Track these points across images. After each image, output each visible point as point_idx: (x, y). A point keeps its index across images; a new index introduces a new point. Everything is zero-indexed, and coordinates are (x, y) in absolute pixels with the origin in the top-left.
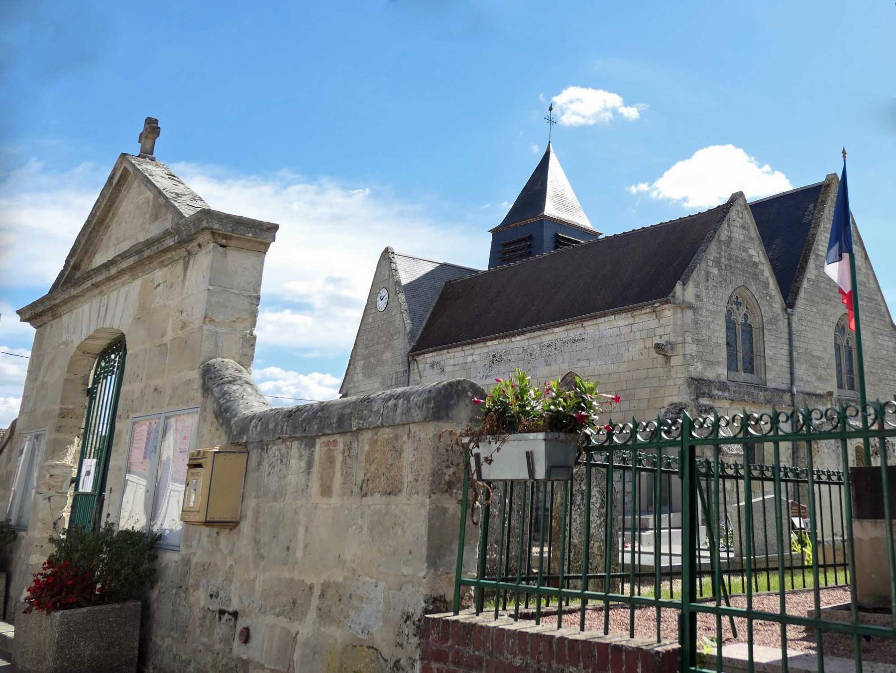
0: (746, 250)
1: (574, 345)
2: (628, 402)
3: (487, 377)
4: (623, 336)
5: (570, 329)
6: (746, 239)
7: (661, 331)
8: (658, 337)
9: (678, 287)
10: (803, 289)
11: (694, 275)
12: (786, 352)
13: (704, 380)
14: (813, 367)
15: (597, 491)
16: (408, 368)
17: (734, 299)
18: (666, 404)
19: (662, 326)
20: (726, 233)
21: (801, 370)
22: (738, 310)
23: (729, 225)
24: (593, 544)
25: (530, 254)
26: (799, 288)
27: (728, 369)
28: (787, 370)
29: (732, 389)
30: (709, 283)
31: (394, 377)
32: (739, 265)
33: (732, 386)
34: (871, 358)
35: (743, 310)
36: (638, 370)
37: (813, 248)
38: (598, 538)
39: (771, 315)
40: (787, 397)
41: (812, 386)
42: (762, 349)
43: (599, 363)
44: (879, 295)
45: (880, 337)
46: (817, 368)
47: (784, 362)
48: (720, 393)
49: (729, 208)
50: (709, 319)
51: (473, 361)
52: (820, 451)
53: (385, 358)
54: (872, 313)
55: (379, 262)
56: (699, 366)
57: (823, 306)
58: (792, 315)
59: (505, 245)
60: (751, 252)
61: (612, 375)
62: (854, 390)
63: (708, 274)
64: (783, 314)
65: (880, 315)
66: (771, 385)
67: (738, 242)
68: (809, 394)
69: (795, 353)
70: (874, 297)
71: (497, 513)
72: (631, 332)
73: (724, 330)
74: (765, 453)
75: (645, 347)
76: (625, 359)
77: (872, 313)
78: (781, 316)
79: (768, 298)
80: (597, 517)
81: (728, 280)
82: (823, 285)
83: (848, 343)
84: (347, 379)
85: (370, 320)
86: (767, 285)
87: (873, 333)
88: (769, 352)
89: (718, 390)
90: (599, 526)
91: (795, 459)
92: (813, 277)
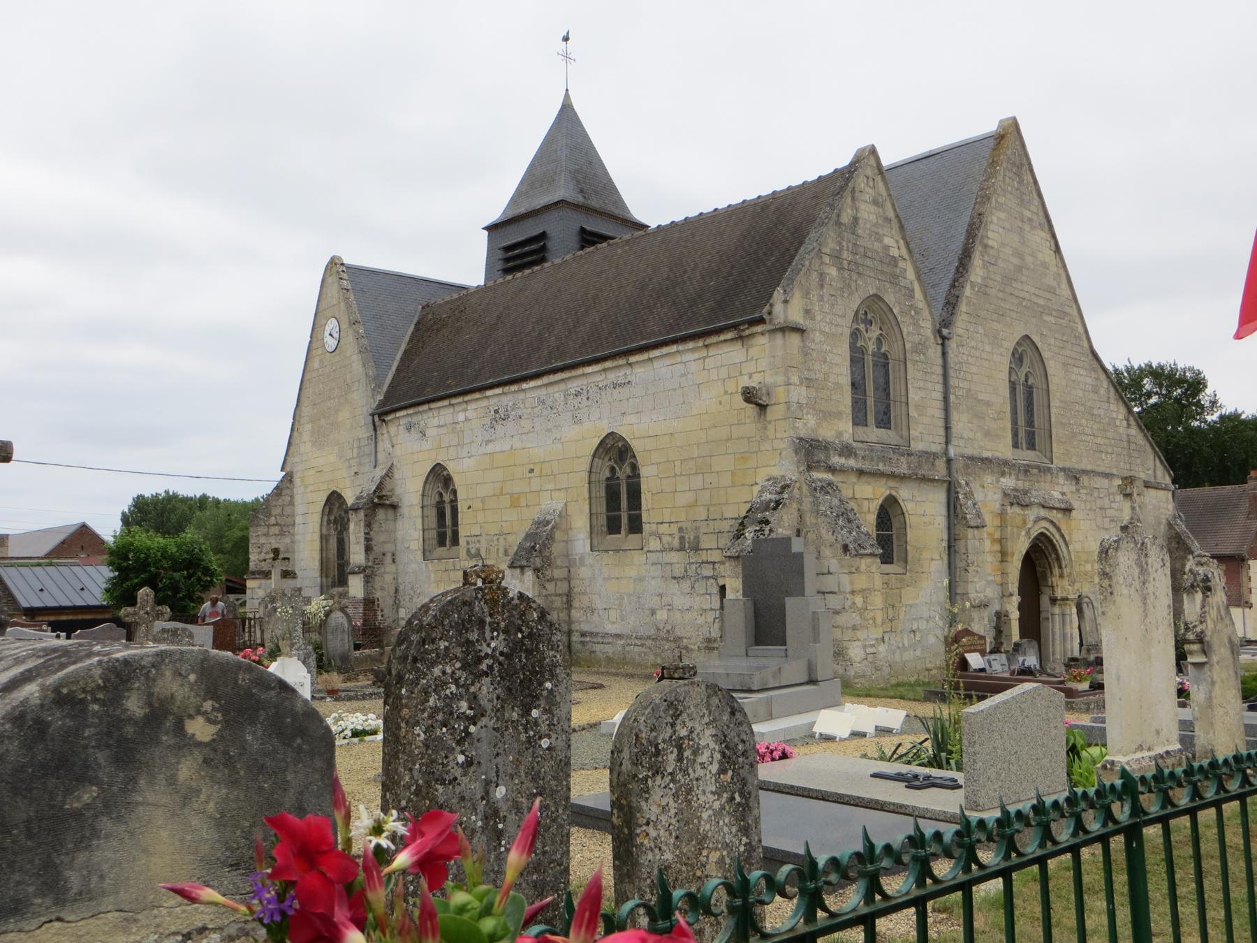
0: (879, 238)
1: (616, 392)
3: (488, 442)
4: (690, 376)
6: (880, 222)
7: (749, 367)
8: (746, 377)
9: (778, 294)
10: (964, 298)
11: (801, 277)
12: (939, 396)
13: (818, 441)
15: (713, 736)
16: (373, 433)
17: (861, 315)
19: (752, 359)
20: (849, 211)
21: (960, 422)
22: (867, 331)
23: (853, 198)
24: (707, 857)
25: (543, 260)
26: (958, 297)
27: (855, 424)
28: (941, 423)
29: (860, 453)
33: (860, 449)
34: (1061, 401)
35: (874, 332)
37: (980, 234)
38: (718, 842)
39: (916, 339)
40: (941, 464)
42: (903, 393)
43: (654, 417)
45: (1075, 369)
47: (936, 410)
48: (842, 461)
50: (824, 347)
51: (467, 420)
52: (1115, 593)
53: (340, 419)
57: (995, 324)
59: (508, 249)
61: (676, 436)
62: (1035, 449)
63: (822, 276)
64: (935, 337)
65: (1075, 337)
66: (917, 446)
67: (868, 226)
68: (972, 458)
69: (952, 397)
70: (1067, 309)
71: (479, 824)
73: (848, 363)
75: (726, 393)
76: (695, 411)
79: (913, 313)
80: (713, 793)
81: (853, 284)
82: (993, 292)
83: (1026, 380)
85: (317, 365)
87: (1065, 365)
88: (914, 396)
89: (840, 455)
90: (719, 813)
92: (979, 281)
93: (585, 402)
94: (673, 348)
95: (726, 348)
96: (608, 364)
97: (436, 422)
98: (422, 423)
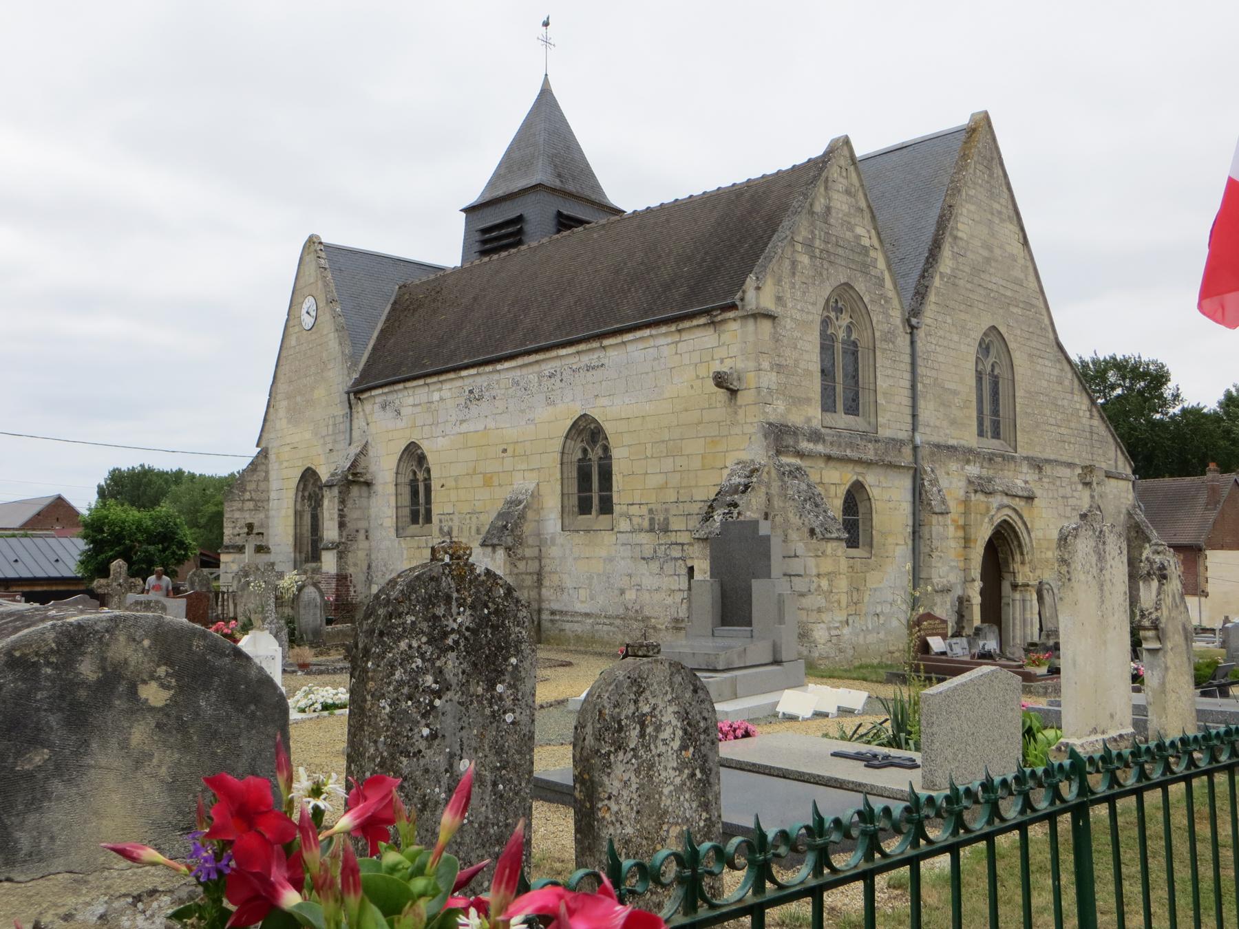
0: (851, 229)
1: (589, 374)
2: (672, 459)
3: (462, 422)
4: (663, 360)
5: (684, 329)
6: (852, 211)
7: (722, 352)
8: (718, 362)
11: (773, 265)
12: (907, 384)
13: (787, 426)
14: (944, 405)
15: (675, 713)
16: (348, 410)
17: (832, 303)
18: (730, 462)
19: (724, 344)
20: (822, 200)
21: (927, 411)
22: (837, 319)
23: (826, 188)
24: (668, 831)
28: (908, 411)
30: (797, 278)
31: (331, 423)
32: (840, 251)
36: (686, 410)
38: (678, 816)
39: (886, 327)
40: (907, 451)
41: (941, 434)
42: (872, 380)
43: (627, 400)
44: (1041, 299)
45: (1040, 360)
46: (950, 407)
47: (904, 398)
48: (811, 446)
49: (827, 162)
51: (442, 399)
54: (1030, 326)
55: (301, 259)
56: (780, 406)
57: (963, 314)
58: (917, 328)
59: (485, 231)
60: (859, 231)
63: (794, 264)
65: (1041, 329)
66: (885, 433)
67: (840, 216)
68: (938, 446)
69: (920, 386)
72: (676, 353)
73: (818, 350)
74: (874, 532)
75: (698, 377)
76: (666, 395)
77: (1030, 326)
78: (901, 329)
79: (883, 302)
81: (825, 272)
82: (961, 283)
84: (266, 427)
85: (293, 343)
86: (880, 283)
87: (1031, 356)
88: (882, 384)
89: (808, 441)
90: (680, 789)
91: (917, 541)
92: (949, 271)
93: (558, 384)
94: (647, 332)
95: (699, 333)
96: (582, 347)
97: (410, 401)
98: (397, 402)
